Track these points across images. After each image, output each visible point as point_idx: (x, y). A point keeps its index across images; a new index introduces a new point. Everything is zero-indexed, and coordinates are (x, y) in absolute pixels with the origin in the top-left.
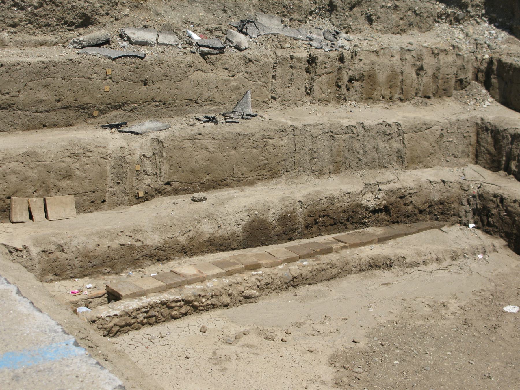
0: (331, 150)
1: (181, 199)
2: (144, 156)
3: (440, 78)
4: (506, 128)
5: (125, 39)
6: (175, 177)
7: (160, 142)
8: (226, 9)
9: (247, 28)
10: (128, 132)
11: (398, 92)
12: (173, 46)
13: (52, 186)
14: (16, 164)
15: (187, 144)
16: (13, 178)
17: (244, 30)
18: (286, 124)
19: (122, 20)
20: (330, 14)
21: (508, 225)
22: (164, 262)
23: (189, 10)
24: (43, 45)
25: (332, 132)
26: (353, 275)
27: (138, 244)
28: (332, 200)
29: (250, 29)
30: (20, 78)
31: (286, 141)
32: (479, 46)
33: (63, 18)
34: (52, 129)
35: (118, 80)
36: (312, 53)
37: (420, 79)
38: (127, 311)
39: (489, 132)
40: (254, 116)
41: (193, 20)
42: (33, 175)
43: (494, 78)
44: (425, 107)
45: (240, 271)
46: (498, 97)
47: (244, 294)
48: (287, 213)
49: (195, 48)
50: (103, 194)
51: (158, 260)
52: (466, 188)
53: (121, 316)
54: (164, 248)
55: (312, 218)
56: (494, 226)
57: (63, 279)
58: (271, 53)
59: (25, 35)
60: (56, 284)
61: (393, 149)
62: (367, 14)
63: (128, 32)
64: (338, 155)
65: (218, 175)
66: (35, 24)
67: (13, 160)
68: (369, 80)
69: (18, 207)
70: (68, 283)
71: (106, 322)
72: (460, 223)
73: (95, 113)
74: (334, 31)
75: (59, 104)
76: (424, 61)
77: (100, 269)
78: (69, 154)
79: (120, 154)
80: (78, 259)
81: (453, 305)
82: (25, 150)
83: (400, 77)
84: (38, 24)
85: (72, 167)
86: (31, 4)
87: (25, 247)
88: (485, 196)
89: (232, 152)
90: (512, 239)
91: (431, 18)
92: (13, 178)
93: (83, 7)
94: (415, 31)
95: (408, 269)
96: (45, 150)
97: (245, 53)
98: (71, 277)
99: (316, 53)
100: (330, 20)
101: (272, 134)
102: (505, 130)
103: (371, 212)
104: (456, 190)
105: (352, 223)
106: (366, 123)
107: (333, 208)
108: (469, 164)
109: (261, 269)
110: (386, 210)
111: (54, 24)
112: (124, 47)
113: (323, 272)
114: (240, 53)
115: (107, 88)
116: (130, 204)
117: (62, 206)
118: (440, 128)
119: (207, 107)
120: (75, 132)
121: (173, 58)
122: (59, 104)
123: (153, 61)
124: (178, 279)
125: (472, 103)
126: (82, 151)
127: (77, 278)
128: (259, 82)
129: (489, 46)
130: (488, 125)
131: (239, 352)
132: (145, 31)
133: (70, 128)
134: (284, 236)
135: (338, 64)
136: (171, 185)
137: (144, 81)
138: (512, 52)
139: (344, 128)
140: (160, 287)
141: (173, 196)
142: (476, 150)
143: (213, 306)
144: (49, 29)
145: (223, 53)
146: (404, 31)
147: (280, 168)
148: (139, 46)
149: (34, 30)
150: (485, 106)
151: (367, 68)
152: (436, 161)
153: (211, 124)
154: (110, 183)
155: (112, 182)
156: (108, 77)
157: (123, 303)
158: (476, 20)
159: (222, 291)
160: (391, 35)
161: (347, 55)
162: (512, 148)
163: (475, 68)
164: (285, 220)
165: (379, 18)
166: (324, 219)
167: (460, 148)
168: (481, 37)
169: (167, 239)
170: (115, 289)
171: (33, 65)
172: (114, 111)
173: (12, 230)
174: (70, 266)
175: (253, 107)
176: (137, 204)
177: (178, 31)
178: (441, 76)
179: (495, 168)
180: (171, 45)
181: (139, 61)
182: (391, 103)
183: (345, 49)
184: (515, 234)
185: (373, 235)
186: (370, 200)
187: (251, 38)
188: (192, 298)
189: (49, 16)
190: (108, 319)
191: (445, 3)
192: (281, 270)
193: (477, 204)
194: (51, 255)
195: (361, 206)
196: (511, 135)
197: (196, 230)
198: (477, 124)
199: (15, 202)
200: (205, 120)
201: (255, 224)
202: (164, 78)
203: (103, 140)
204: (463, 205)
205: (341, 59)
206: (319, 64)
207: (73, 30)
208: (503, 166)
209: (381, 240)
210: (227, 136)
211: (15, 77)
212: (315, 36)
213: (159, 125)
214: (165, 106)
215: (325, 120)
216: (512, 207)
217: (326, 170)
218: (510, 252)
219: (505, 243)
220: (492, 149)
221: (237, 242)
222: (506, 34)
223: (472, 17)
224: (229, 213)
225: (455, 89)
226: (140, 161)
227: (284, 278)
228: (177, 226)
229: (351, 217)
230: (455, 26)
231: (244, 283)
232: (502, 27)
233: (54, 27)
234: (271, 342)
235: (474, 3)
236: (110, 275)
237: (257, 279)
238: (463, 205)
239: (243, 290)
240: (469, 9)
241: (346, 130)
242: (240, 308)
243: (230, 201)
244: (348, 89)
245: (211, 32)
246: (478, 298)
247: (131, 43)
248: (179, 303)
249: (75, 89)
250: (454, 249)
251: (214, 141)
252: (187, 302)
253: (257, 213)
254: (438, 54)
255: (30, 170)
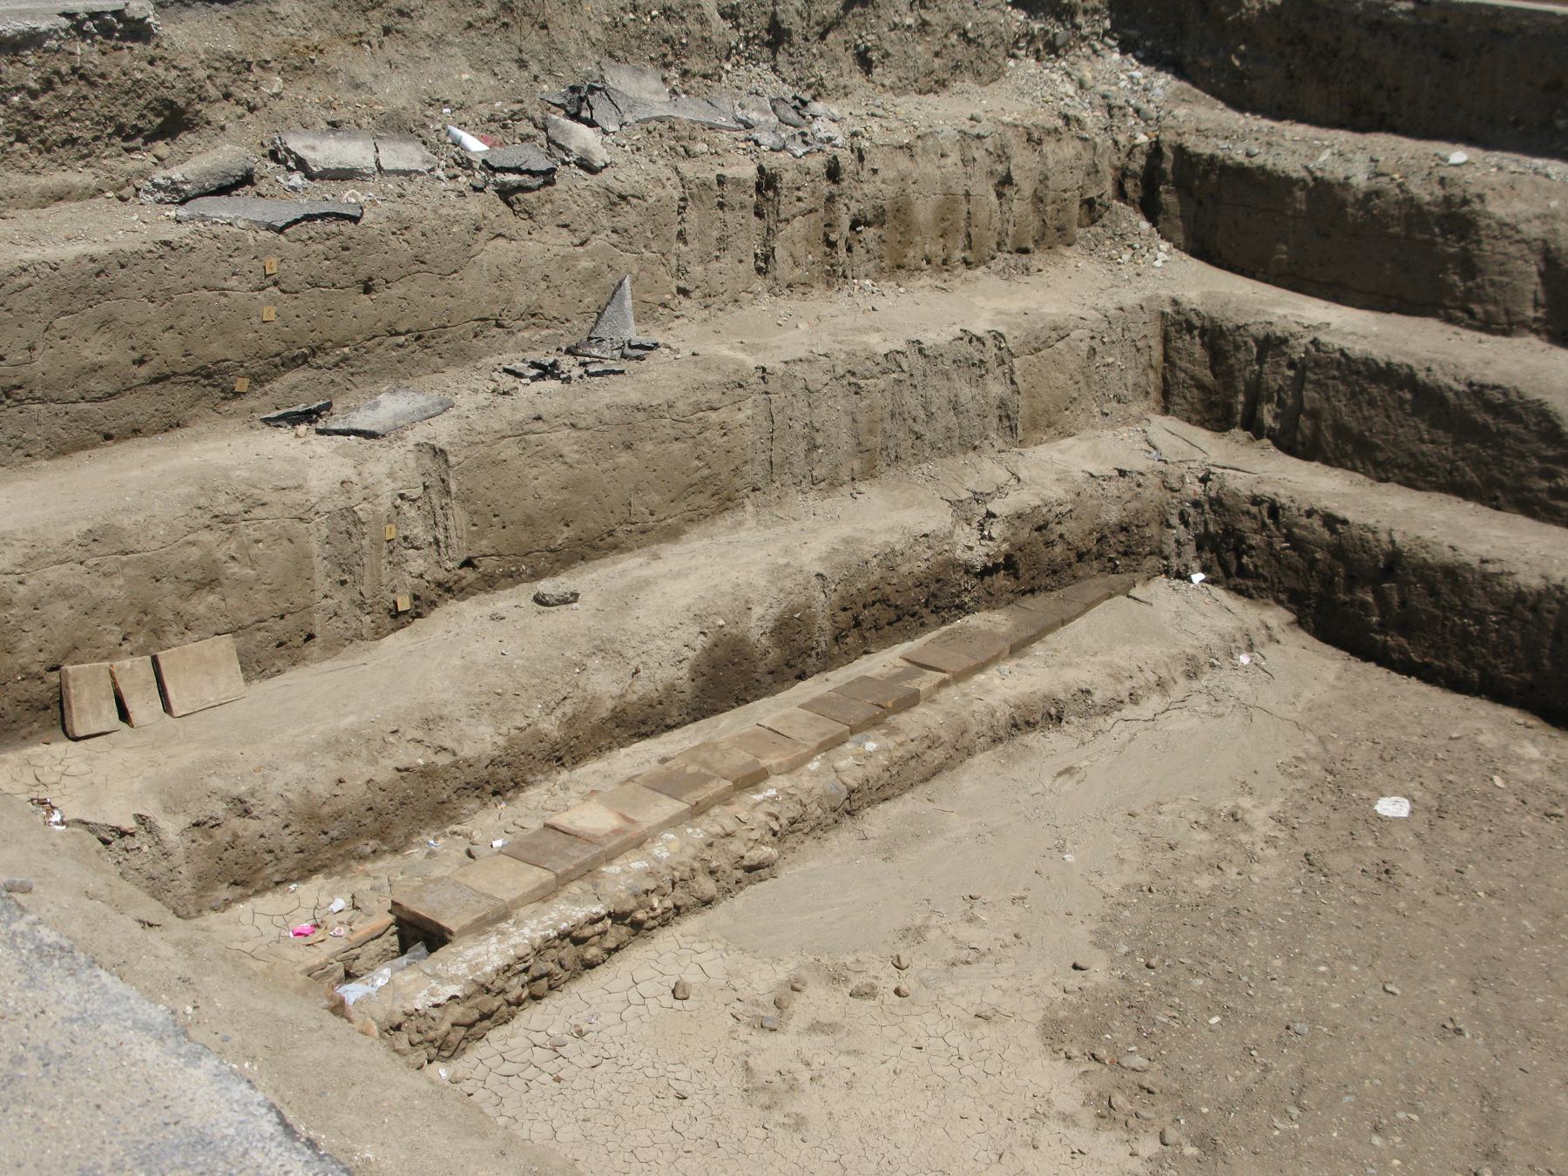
0: (854, 421)
1: (508, 601)
2: (402, 496)
3: (1048, 200)
4: (1242, 322)
5: (291, 164)
6: (485, 542)
7: (438, 453)
8: (525, 57)
9: (591, 108)
10: (346, 433)
11: (961, 245)
12: (421, 174)
13: (170, 616)
14: (64, 568)
15: (509, 450)
16: (61, 611)
17: (585, 114)
18: (742, 363)
19: (266, 110)
20: (774, 54)
21: (1296, 571)
22: (509, 794)
23: (434, 69)
24: (61, 199)
25: (853, 374)
26: (980, 758)
27: (443, 760)
28: (889, 559)
29: (601, 109)
30: (32, 309)
31: (749, 412)
32: (1116, 111)
33: (111, 119)
34: (128, 443)
35: (297, 287)
36: (764, 164)
37: (1005, 208)
38: (482, 980)
39: (1196, 332)
40: (650, 348)
41: (447, 96)
42: (114, 592)
43: (1168, 192)
44: (1028, 279)
45: (724, 799)
46: (1180, 238)
47: (745, 863)
48: (793, 610)
49: (479, 176)
50: (307, 618)
51: (495, 793)
52: (1176, 485)
53: (468, 997)
54: (508, 759)
55: (849, 613)
56: (1259, 576)
57: (257, 893)
58: (668, 172)
59: (9, 174)
60: (242, 908)
61: (991, 401)
62: (856, 47)
63: (298, 144)
64: (870, 431)
65: (594, 523)
66: (33, 141)
67: (54, 558)
68: (895, 223)
69: (86, 694)
70: (270, 903)
71: (432, 1023)
72: (1167, 572)
73: (242, 384)
74: (795, 98)
75: (144, 371)
76: (1013, 162)
77: (351, 847)
78: (206, 520)
79: (341, 502)
80: (292, 829)
81: (1259, 817)
82: (85, 526)
83: (964, 207)
84: (43, 142)
85: (219, 555)
86: (19, 84)
87: (141, 819)
88: (1228, 501)
89: (624, 458)
90: (1308, 606)
91: (1002, 48)
92: (61, 611)
93: (162, 84)
94: (968, 83)
95: (1101, 720)
96: (141, 518)
97: (606, 177)
98: (277, 883)
99: (775, 164)
100: (774, 69)
101: (714, 396)
102: (1239, 328)
103: (976, 575)
104: (1152, 492)
105: (936, 610)
106: (929, 339)
107: (895, 581)
108: (1151, 416)
109: (770, 782)
110: (1009, 565)
111: (89, 136)
112: (294, 189)
113: (912, 763)
114: (593, 180)
115: (269, 313)
116: (378, 634)
117: (205, 671)
118: (1088, 333)
119: (526, 334)
120: (196, 447)
121: (435, 211)
122: (144, 371)
123: (386, 225)
124: (581, 854)
125: (1126, 257)
126: (239, 507)
127: (292, 881)
128: (647, 254)
129: (1137, 111)
130: (1193, 315)
131: (808, 1055)
132: (341, 139)
133: (178, 433)
134: (787, 670)
135: (826, 187)
136: (475, 567)
137: (365, 283)
138: (1209, 125)
139: (880, 359)
140: (543, 886)
141: (482, 596)
142: (1164, 378)
143: (678, 910)
144: (73, 152)
145: (552, 183)
146: (943, 84)
147: (738, 482)
148: (333, 184)
149: (34, 158)
150: (1158, 264)
151: (890, 191)
152: (1082, 417)
153: (551, 385)
154: (323, 584)
155: (327, 584)
156: (269, 282)
157: (458, 954)
158: (1092, 46)
159: (696, 865)
160: (917, 98)
161: (846, 159)
162: (1261, 372)
163: (1116, 169)
164: (789, 631)
165: (887, 55)
166: (873, 610)
167: (1130, 378)
168: (1113, 88)
169: (513, 732)
170: (422, 909)
171: (64, 270)
172: (284, 372)
173: (84, 768)
174: (271, 851)
175: (638, 321)
176: (394, 630)
177: (423, 132)
178: (1051, 196)
179: (1218, 421)
180: (417, 172)
181: (348, 228)
182: (946, 275)
183: (835, 146)
184: (1316, 594)
185: (991, 637)
186: (971, 548)
187: (606, 133)
188: (632, 903)
189: (73, 114)
190: (435, 1013)
191: (1024, 9)
192: (816, 775)
193: (1206, 523)
194: (217, 832)
195: (954, 565)
196: (1256, 340)
197: (580, 693)
198: (1163, 314)
199: (75, 680)
200: (534, 372)
201: (719, 652)
202: (415, 268)
203: (288, 467)
204: (1170, 526)
205: (833, 172)
206: (784, 192)
207: (138, 149)
208: (1239, 418)
209: (1018, 648)
210: (607, 415)
211: (16, 308)
212: (754, 116)
213: (421, 401)
214: (422, 345)
215: (824, 343)
216: (1304, 527)
217: (845, 475)
218: (1305, 638)
219: (1290, 617)
220: (1206, 376)
221: (680, 708)
222: (1169, 77)
223: (1084, 38)
224: (655, 632)
225: (1080, 226)
226: (394, 512)
227: (830, 797)
228: (531, 690)
229: (934, 595)
230: (1049, 65)
231: (742, 832)
232: (1152, 59)
233: (87, 145)
234: (871, 1002)
235: (1089, 5)
236: (379, 857)
237: (770, 814)
238: (1170, 526)
239: (743, 851)
240: (1080, 20)
241: (885, 364)
242: (741, 900)
243: (642, 596)
244: (849, 249)
245: (505, 126)
246: (1300, 784)
247: (310, 176)
248: (600, 924)
249: (184, 323)
250: (1190, 651)
251: (575, 434)
252: (617, 917)
253: (721, 622)
254: (1040, 142)
255: (103, 581)
